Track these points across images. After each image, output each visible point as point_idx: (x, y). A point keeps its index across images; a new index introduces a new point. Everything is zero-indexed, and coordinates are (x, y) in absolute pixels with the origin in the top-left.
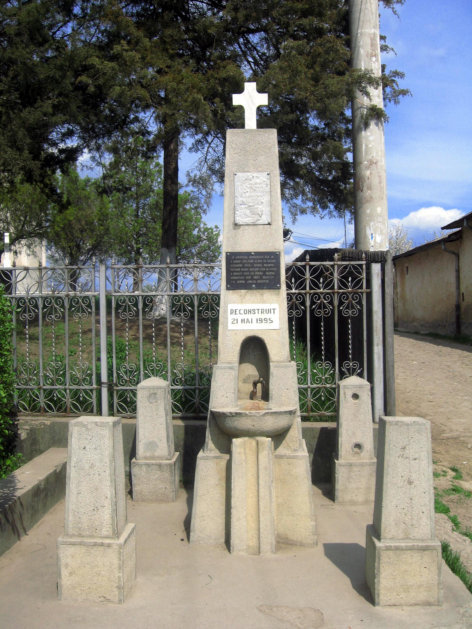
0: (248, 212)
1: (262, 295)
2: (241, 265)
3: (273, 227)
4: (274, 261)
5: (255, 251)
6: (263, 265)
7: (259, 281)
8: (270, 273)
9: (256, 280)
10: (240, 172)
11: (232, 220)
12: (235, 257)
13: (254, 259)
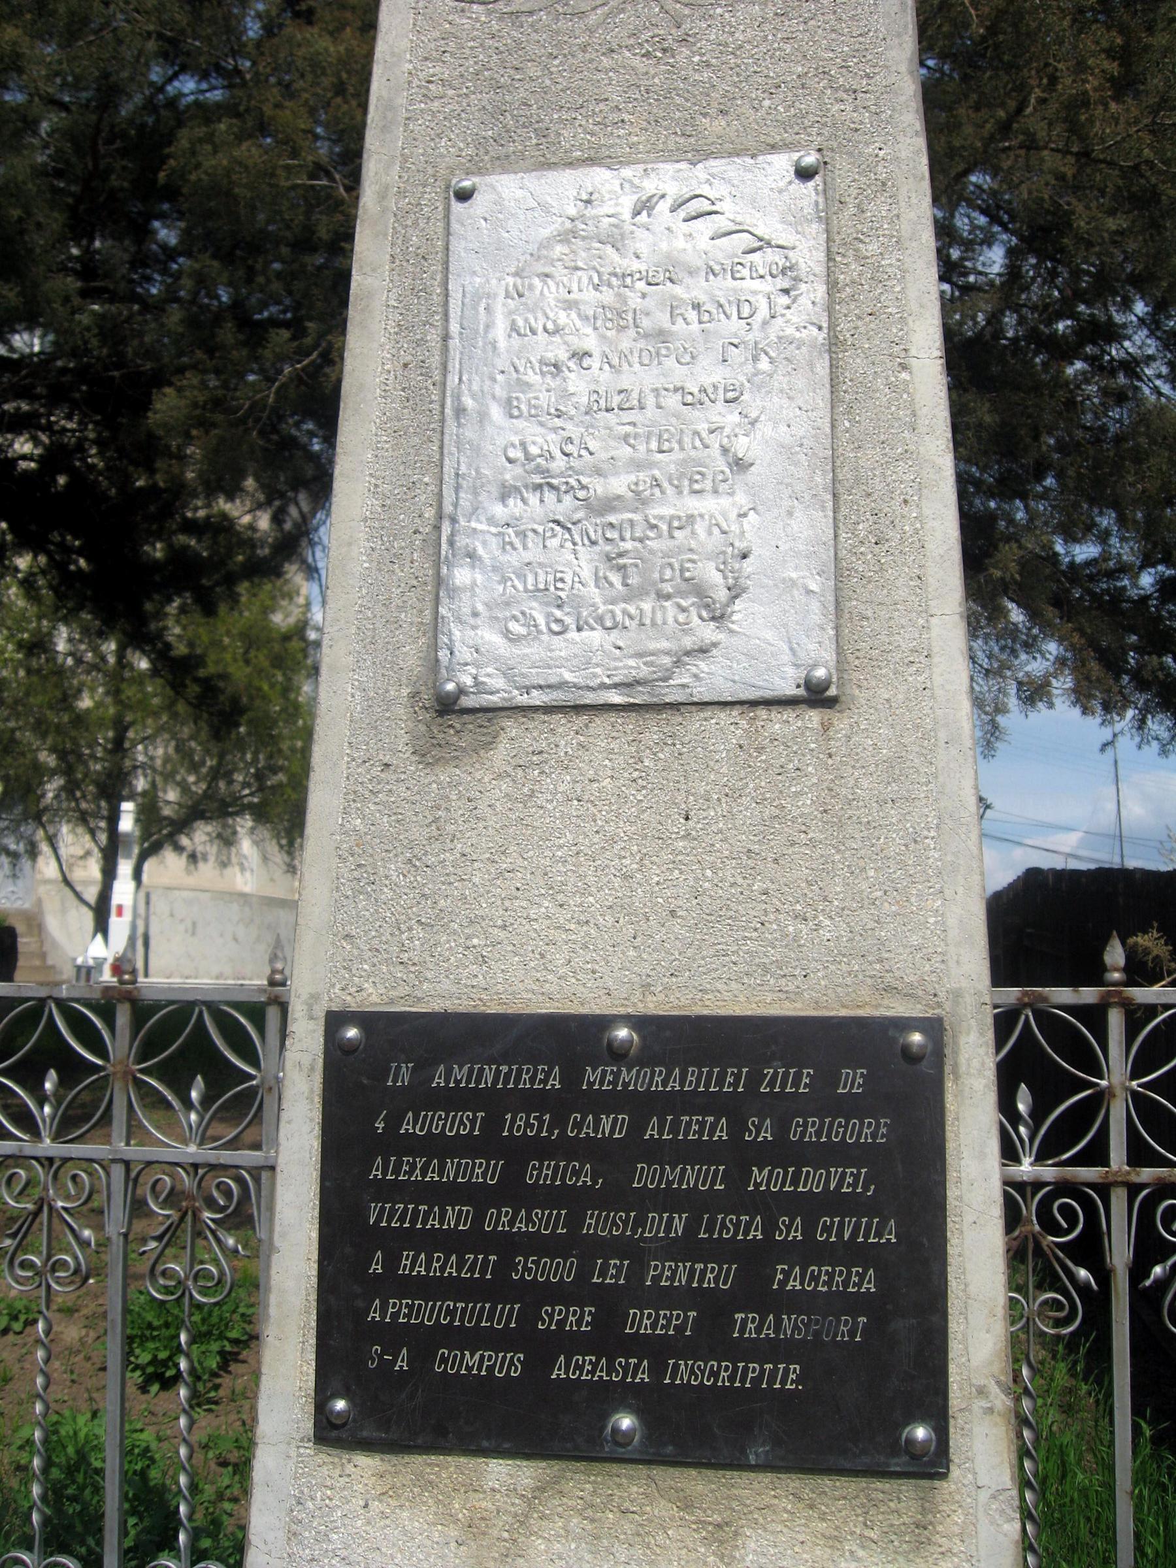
0: (580, 565)
1: (722, 1535)
2: (482, 1171)
3: (862, 727)
4: (869, 1131)
5: (652, 1006)
6: (738, 1176)
7: (686, 1372)
8: (824, 1278)
9: (657, 1351)
10: (504, 164)
11: (411, 657)
12: (424, 1067)
13: (641, 1105)
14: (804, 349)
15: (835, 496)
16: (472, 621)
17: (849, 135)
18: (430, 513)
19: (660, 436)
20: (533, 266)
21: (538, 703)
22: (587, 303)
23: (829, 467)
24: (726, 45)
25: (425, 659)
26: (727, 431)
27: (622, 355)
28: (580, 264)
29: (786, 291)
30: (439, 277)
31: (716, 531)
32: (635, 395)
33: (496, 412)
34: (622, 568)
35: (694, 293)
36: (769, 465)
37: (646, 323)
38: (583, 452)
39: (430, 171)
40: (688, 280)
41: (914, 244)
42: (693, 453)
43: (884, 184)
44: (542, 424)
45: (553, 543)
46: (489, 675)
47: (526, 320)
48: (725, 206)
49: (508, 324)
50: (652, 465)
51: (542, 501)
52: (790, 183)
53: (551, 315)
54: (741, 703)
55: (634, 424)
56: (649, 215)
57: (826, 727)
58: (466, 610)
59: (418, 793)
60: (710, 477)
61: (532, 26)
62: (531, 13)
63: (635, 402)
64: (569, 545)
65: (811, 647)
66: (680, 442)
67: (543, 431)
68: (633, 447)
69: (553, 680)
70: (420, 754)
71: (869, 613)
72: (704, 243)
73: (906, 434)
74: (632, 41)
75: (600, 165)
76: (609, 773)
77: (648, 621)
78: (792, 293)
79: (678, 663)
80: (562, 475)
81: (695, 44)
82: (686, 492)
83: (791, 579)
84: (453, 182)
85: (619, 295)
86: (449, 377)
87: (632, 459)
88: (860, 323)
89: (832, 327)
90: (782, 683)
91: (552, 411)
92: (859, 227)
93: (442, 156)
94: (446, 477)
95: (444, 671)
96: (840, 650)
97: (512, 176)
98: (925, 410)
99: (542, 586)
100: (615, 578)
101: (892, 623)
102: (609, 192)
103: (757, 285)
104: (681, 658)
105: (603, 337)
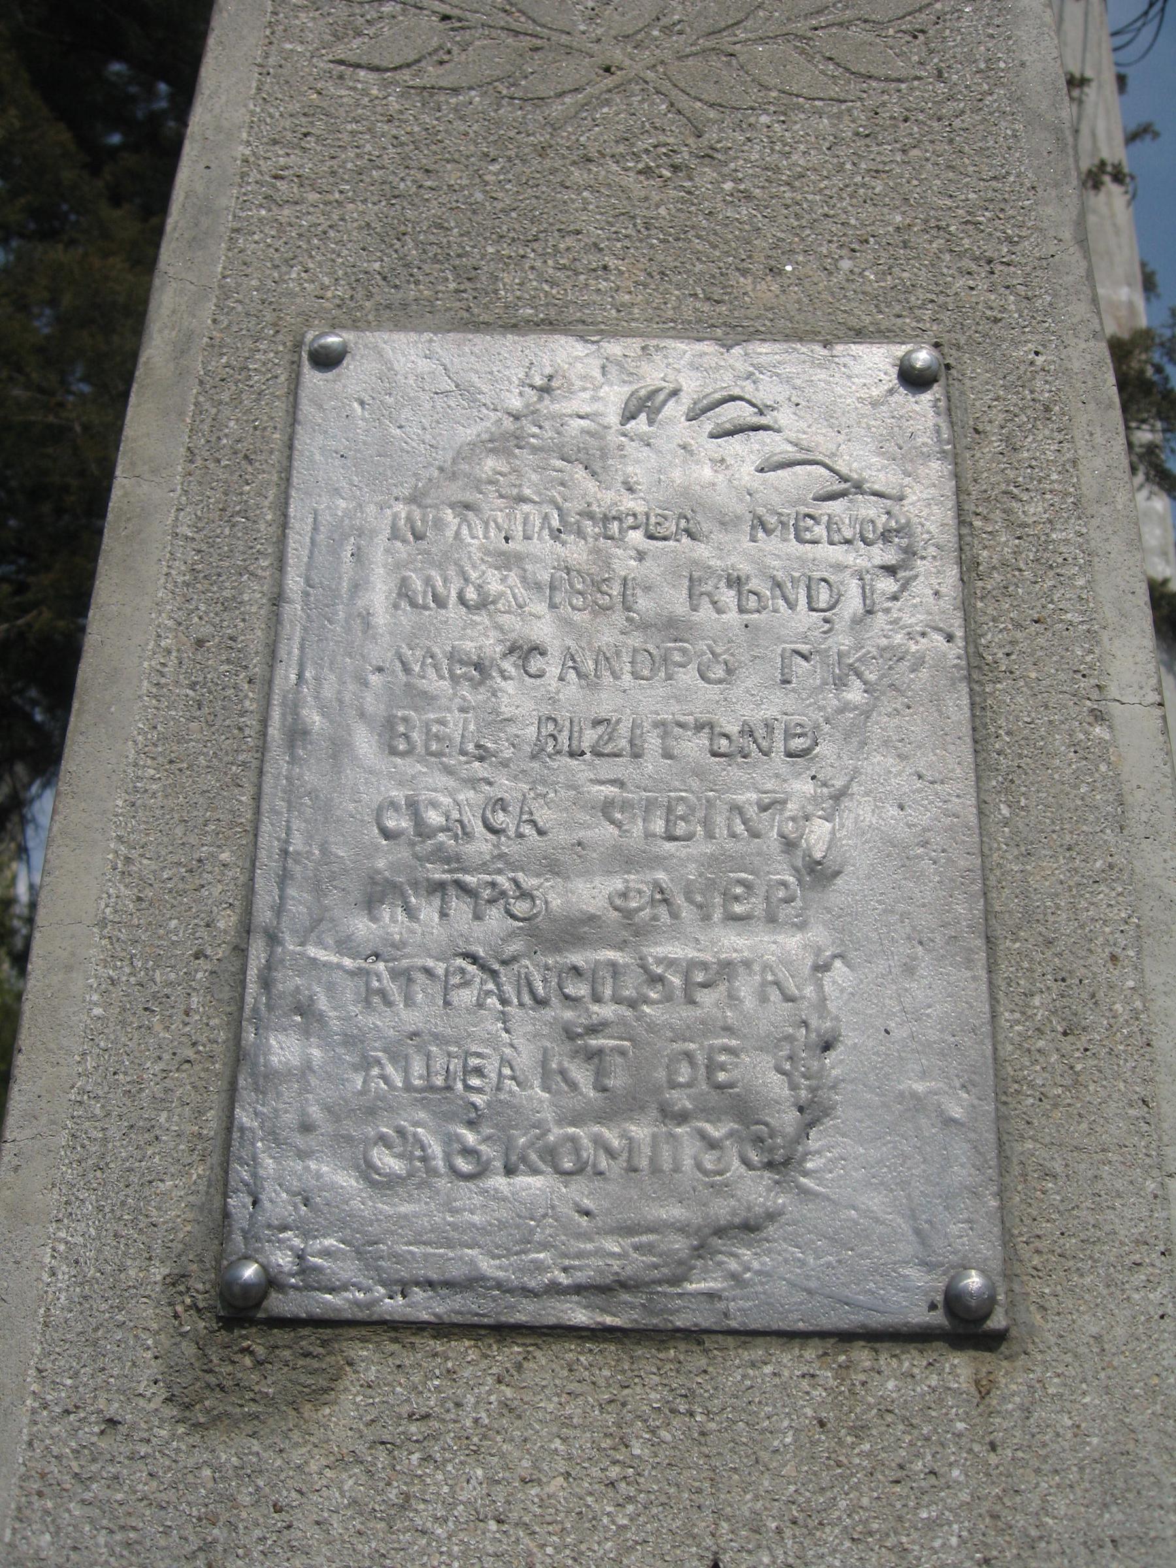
0: (511, 1046)
10: (400, 316)
11: (175, 1202)
14: (924, 673)
15: (990, 941)
16: (299, 1140)
17: (984, 326)
18: (227, 921)
19: (670, 810)
20: (449, 488)
21: (425, 1316)
22: (537, 560)
23: (977, 887)
24: (777, 170)
25: (201, 1208)
26: (792, 807)
27: (602, 658)
28: (527, 492)
29: (891, 570)
30: (271, 493)
31: (774, 995)
32: (624, 729)
33: (365, 743)
34: (593, 1056)
35: (732, 560)
36: (868, 877)
37: (643, 603)
38: (527, 829)
39: (269, 316)
40: (718, 536)
41: (1104, 510)
42: (730, 845)
43: (1047, 409)
44: (449, 771)
45: (466, 997)
46: (326, 1253)
47: (428, 581)
48: (783, 417)
49: (393, 585)
50: (658, 861)
51: (443, 915)
52: (891, 392)
53: (474, 575)
54: (823, 1335)
55: (620, 783)
56: (651, 422)
57: (984, 1389)
58: (290, 1118)
59: (174, 1485)
60: (761, 891)
61: (456, 110)
62: (455, 91)
63: (623, 743)
64: (493, 1001)
65: (954, 1229)
66: (706, 823)
67: (451, 783)
68: (618, 825)
69: (456, 1272)
70: (182, 1403)
71: (1058, 1167)
72: (746, 473)
73: (1109, 835)
74: (621, 149)
75: (566, 332)
76: (562, 1466)
77: (644, 1163)
78: (901, 574)
79: (701, 1250)
80: (483, 868)
81: (726, 164)
82: (717, 915)
83: (914, 1095)
84: (310, 336)
85: (596, 551)
86: (280, 670)
87: (617, 849)
88: (1019, 635)
89: (972, 636)
90: (898, 1299)
91: (470, 747)
92: (1011, 474)
93: (291, 294)
94: (262, 854)
95: (238, 1237)
96: (1007, 1238)
97: (413, 336)
98: (1139, 795)
99: (439, 1081)
100: (582, 1075)
101: (1099, 1186)
102: (584, 378)
103: (837, 553)
104: (710, 1239)
105: (567, 623)
